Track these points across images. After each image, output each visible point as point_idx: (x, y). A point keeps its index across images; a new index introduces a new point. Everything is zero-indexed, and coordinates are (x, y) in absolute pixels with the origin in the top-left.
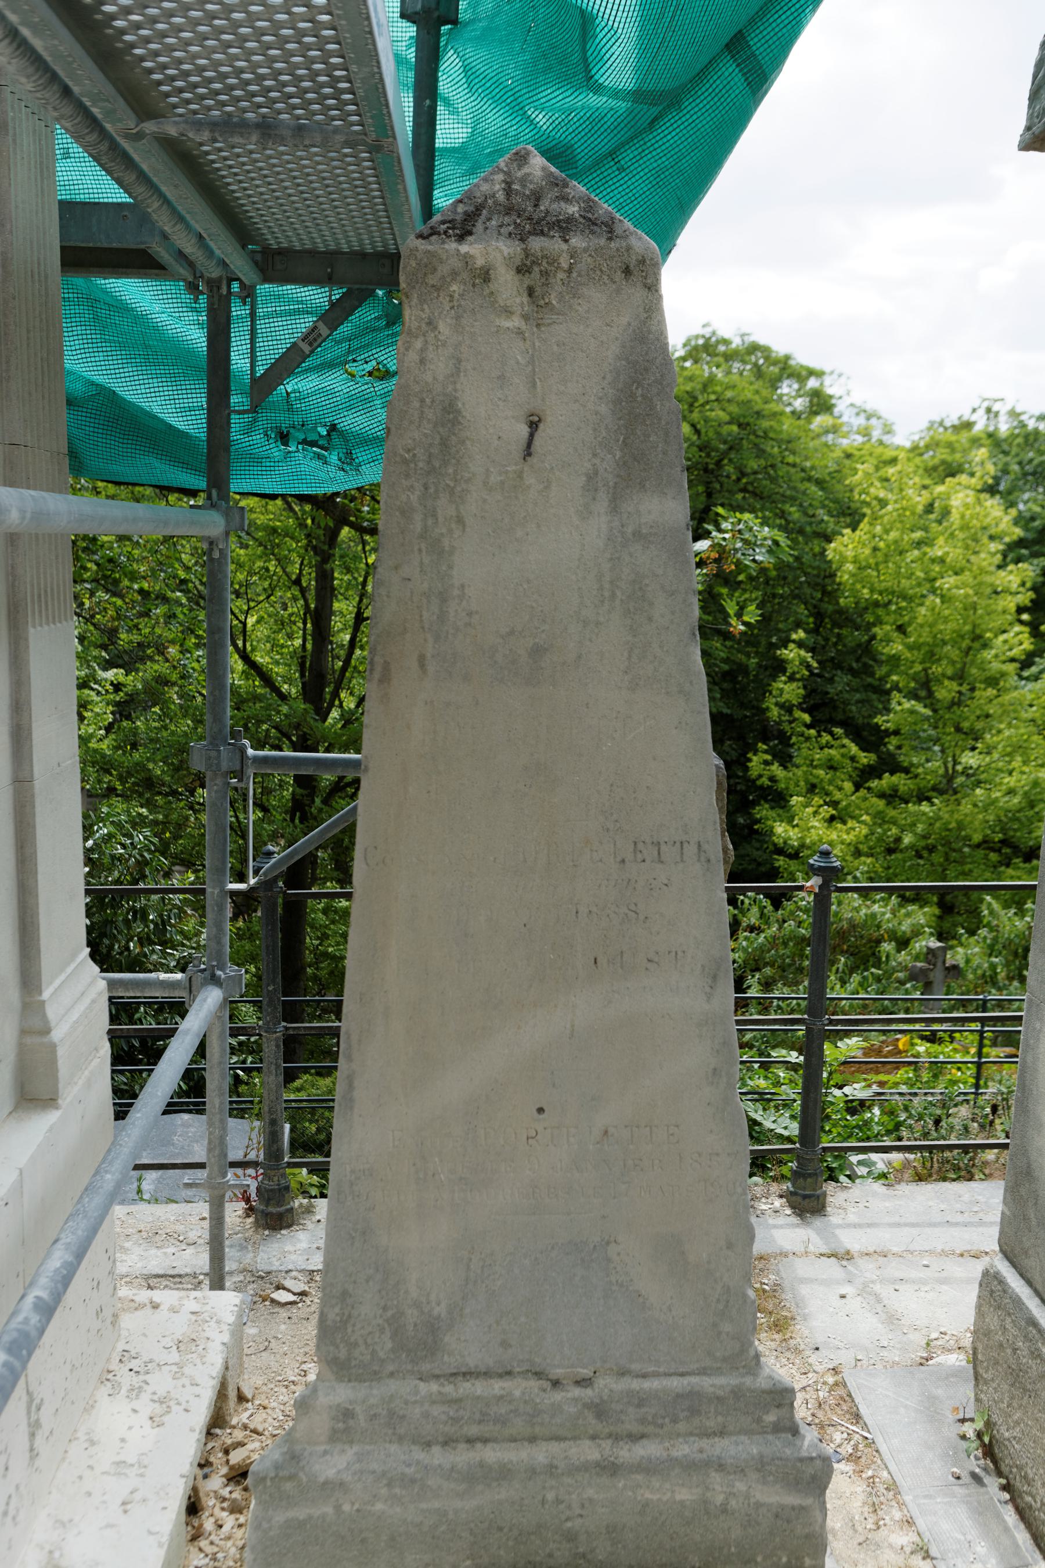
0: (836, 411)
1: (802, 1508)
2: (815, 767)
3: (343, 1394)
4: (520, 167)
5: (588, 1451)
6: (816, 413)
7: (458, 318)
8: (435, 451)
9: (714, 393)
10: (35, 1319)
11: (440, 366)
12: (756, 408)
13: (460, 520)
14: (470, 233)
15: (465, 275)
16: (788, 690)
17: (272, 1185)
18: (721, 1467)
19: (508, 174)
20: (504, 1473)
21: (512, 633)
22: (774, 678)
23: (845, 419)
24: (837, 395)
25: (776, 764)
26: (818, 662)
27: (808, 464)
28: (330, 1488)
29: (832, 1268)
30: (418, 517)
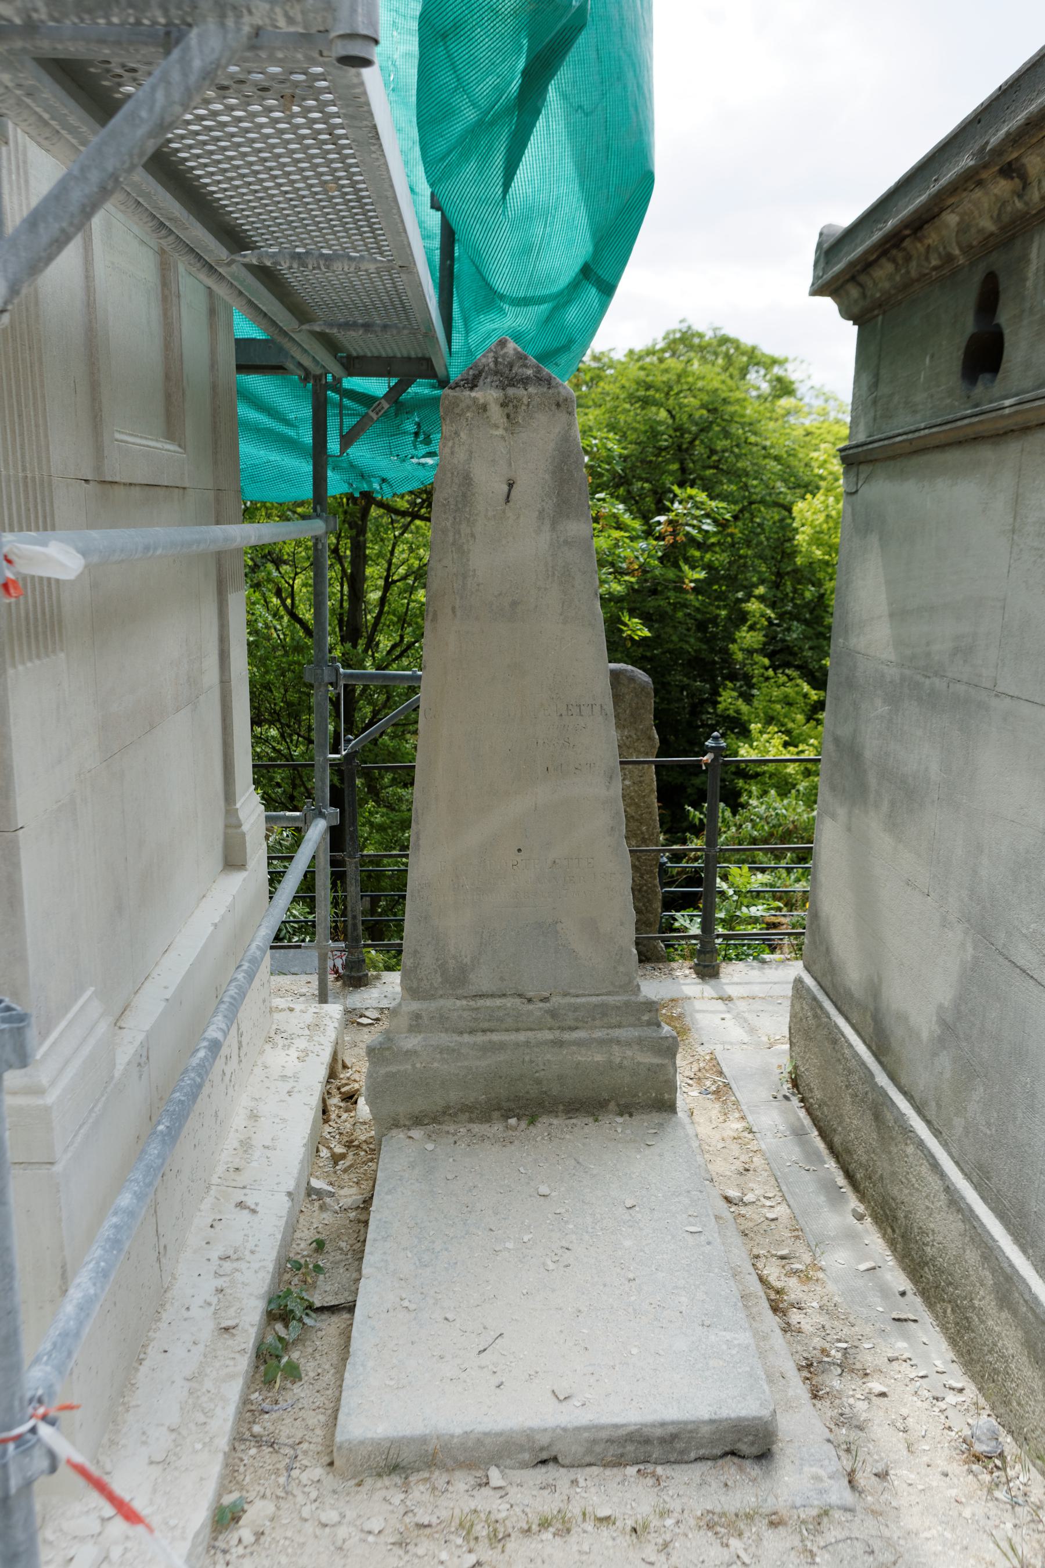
0: (799, 394)
1: (663, 1065)
2: (774, 702)
3: (415, 1006)
4: (502, 349)
5: (548, 1035)
6: (779, 397)
7: (470, 430)
8: (459, 499)
9: (687, 383)
10: (258, 953)
11: (461, 455)
12: (723, 395)
13: (473, 536)
14: (476, 386)
15: (474, 408)
16: (748, 638)
17: (354, 958)
18: (618, 1042)
19: (496, 352)
20: (502, 1046)
21: (500, 594)
22: (737, 627)
23: (806, 400)
24: (801, 378)
25: (740, 700)
26: (776, 614)
27: (768, 443)
28: (409, 1054)
29: (720, 1005)
30: (451, 534)
